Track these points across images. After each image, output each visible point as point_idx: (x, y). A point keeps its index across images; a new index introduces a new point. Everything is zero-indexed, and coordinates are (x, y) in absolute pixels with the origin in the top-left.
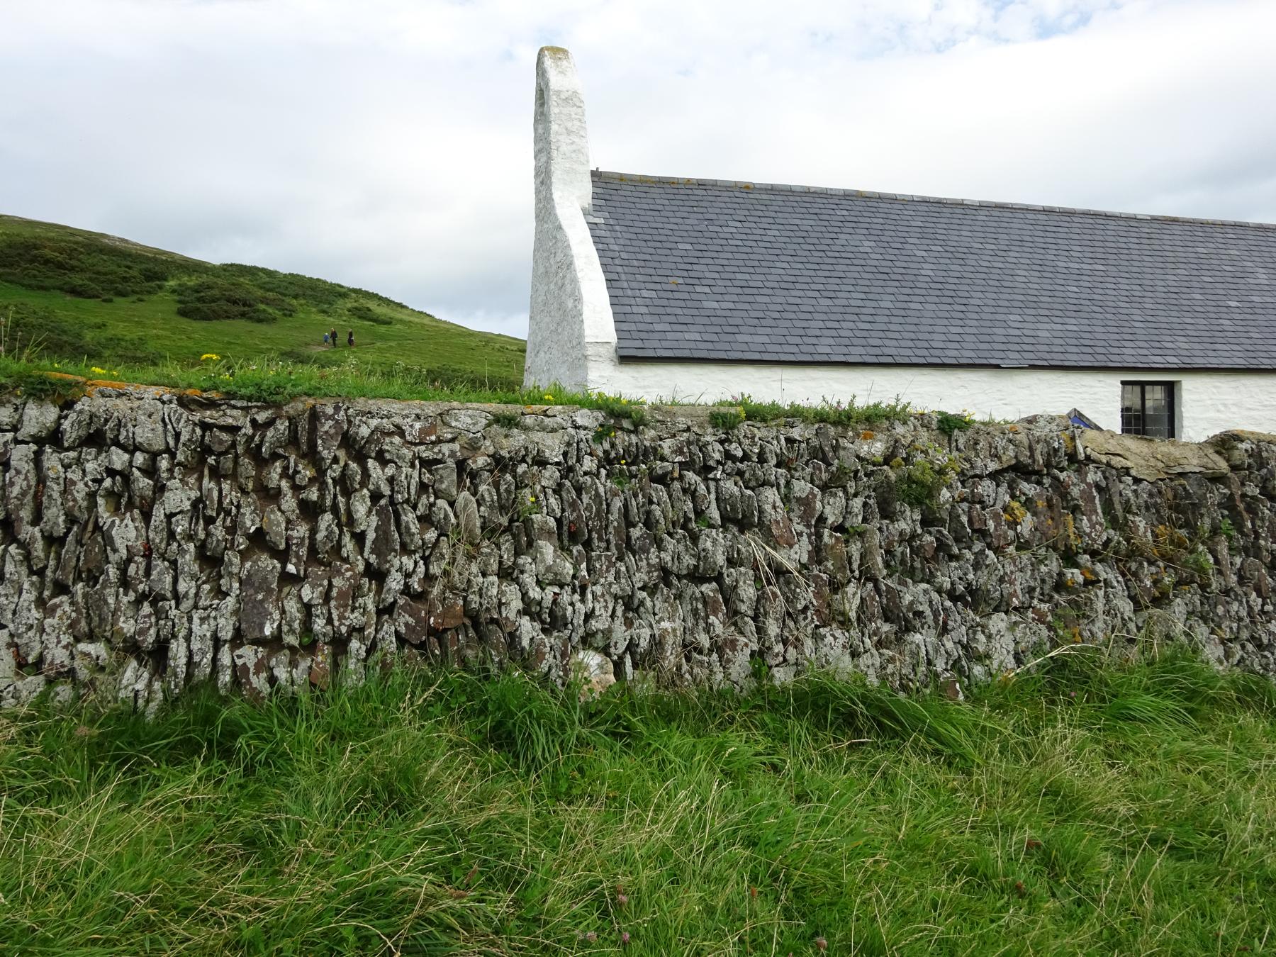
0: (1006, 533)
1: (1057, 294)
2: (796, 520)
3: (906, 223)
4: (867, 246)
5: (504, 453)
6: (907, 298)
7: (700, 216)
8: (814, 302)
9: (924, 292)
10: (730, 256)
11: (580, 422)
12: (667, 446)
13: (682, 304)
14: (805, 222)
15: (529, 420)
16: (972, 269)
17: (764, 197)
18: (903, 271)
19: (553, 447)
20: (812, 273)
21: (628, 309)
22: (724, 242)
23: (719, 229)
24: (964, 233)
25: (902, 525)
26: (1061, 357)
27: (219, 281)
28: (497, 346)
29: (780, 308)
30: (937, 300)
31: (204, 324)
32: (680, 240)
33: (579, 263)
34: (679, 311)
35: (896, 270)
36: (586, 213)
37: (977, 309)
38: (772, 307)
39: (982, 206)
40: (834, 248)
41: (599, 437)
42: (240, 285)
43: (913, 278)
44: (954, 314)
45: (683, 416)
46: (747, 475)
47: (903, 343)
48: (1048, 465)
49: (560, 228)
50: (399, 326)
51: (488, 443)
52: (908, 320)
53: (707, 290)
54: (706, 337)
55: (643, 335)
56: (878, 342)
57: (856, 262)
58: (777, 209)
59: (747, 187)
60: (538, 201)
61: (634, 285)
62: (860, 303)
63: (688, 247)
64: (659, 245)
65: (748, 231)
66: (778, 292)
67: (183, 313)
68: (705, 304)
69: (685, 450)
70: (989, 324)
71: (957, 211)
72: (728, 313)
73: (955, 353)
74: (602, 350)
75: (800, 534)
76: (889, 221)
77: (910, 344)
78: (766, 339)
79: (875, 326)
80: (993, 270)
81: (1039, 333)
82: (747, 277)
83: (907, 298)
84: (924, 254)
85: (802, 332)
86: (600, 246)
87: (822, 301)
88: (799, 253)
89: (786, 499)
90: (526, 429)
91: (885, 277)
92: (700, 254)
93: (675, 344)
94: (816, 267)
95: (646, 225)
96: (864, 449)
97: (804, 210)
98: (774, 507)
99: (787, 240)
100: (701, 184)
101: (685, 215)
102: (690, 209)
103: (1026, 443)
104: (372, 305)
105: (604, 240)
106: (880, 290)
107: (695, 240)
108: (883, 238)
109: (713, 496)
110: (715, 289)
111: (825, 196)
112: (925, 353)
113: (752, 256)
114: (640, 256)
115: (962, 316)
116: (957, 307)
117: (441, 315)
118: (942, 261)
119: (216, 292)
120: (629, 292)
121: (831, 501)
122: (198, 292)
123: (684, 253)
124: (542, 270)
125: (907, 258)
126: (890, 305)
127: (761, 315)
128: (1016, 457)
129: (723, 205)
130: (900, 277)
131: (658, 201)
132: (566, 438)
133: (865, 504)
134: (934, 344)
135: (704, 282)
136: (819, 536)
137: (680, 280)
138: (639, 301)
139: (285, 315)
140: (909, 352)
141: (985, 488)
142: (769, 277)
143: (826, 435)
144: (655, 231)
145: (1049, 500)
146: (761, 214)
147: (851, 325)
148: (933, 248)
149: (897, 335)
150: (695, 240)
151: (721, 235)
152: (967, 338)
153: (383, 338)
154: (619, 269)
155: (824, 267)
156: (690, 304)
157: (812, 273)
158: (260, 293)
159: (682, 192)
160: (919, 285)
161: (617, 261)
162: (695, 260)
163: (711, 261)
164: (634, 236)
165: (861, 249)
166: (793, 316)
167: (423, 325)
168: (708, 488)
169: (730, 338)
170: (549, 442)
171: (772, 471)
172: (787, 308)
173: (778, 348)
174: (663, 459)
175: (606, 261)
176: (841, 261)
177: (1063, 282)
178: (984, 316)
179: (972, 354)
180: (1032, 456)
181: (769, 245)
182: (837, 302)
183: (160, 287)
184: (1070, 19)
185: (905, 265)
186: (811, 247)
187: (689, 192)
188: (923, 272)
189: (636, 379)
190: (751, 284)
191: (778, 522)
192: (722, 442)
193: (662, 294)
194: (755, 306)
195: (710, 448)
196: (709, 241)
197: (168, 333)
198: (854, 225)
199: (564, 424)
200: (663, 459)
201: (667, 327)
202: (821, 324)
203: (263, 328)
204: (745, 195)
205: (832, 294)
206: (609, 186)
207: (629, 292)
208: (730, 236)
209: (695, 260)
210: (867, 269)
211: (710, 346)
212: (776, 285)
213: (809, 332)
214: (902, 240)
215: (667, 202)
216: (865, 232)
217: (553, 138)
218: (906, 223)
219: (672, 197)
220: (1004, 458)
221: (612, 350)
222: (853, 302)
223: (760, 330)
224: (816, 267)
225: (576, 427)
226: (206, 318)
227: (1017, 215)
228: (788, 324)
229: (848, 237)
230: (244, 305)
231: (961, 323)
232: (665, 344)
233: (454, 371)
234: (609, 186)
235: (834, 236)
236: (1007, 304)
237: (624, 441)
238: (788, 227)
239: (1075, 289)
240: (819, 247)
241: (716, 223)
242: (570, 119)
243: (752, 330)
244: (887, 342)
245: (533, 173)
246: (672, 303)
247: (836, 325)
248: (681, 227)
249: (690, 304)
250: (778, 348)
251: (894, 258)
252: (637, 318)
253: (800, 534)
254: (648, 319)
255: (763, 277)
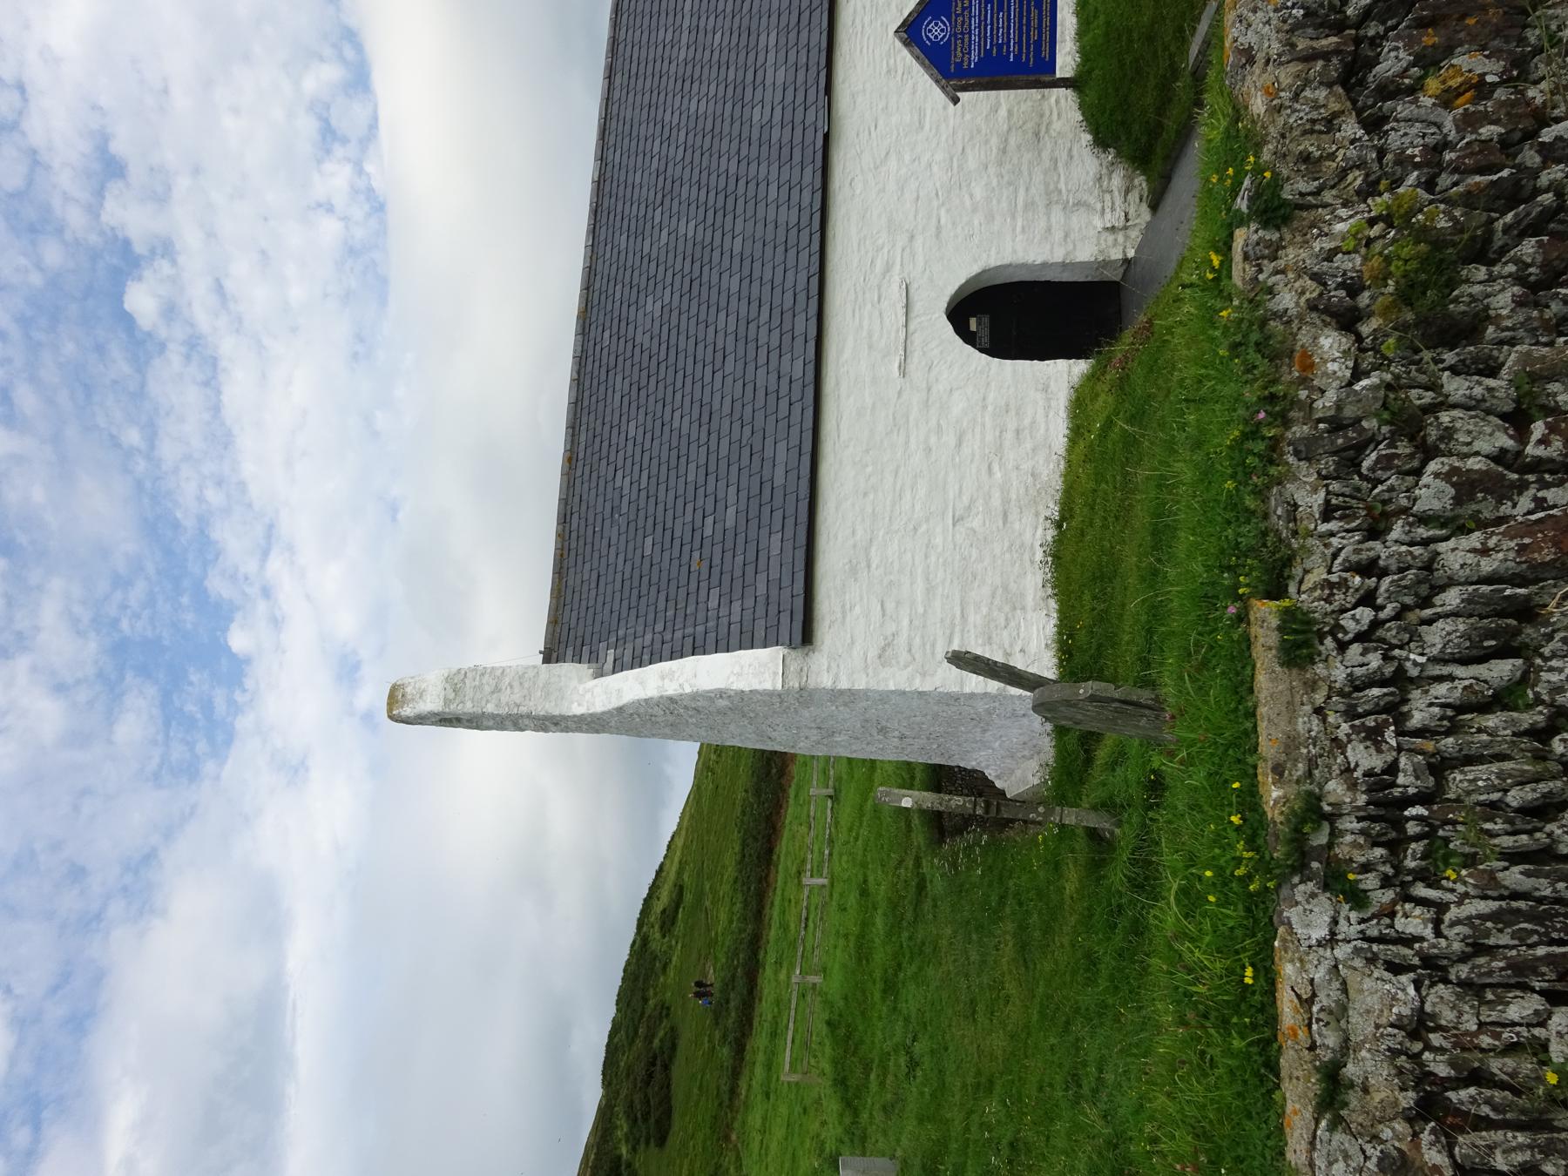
0: (1502, 104)
1: (724, 59)
2: (1506, 509)
3: (623, 254)
4: (652, 306)
5: (1408, 1099)
6: (727, 256)
7: (607, 523)
8: (729, 380)
9: (718, 234)
10: (662, 487)
11: (1320, 932)
12: (1364, 757)
13: (729, 555)
14: (618, 387)
15: (1331, 1039)
16: (688, 170)
17: (583, 438)
18: (688, 260)
19: (1381, 998)
20: (689, 381)
21: (735, 628)
22: (643, 494)
23: (625, 500)
24: (638, 181)
25: (1503, 301)
26: (814, 52)
27: (623, 1093)
28: (713, 757)
29: (737, 425)
30: (729, 218)
31: (676, 1116)
32: (639, 552)
33: (671, 689)
34: (739, 559)
35: (687, 269)
36: (600, 674)
37: (744, 163)
38: (735, 436)
39: (602, 158)
40: (655, 350)
41: (1358, 899)
42: (629, 1068)
43: (699, 248)
44: (751, 193)
45: (1292, 720)
46: (1408, 600)
47: (791, 262)
48: (1339, 27)
49: (620, 710)
50: (686, 877)
51: (1387, 1134)
52: (757, 255)
53: (709, 520)
54: (777, 526)
55: (773, 609)
56: (789, 295)
57: (674, 322)
58: (599, 422)
59: (570, 460)
60: (579, 730)
61: (701, 617)
62: (732, 319)
63: (649, 541)
64: (645, 580)
65: (629, 461)
66: (715, 426)
67: (662, 1140)
68: (730, 523)
69: (1370, 722)
70: (765, 148)
71: (607, 189)
72: (743, 494)
73: (807, 194)
74: (793, 667)
75: (1540, 504)
76: (620, 277)
77: (792, 253)
78: (782, 446)
79: (766, 297)
80: (690, 143)
81: (780, 82)
82: (692, 466)
83: (727, 256)
84: (665, 233)
85: (772, 398)
86: (646, 657)
87: (729, 368)
88: (660, 396)
89: (1457, 527)
90: (1346, 1047)
91: (696, 284)
92: (659, 528)
93: (787, 570)
94: (680, 374)
95: (618, 595)
96: (1339, 368)
97: (602, 388)
98: (1485, 551)
99: (642, 411)
100: (564, 518)
101: (605, 542)
102: (598, 535)
103: (1294, 68)
104: (658, 907)
105: (638, 652)
106: (714, 291)
107: (640, 532)
108: (643, 286)
109: (1459, 671)
110: (710, 508)
111: (582, 360)
112: (805, 234)
113: (664, 459)
114: (661, 605)
115: (752, 185)
116: (741, 190)
117: (670, 821)
118: (675, 210)
119: (637, 1098)
120: (711, 624)
121: (1463, 438)
122: (636, 1120)
123: (658, 548)
124: (667, 731)
125: (671, 255)
126: (736, 278)
127: (746, 452)
128: (1330, 85)
129: (593, 492)
130: (697, 265)
131: (586, 577)
132: (1358, 963)
133: (1454, 371)
134: (793, 220)
135: (698, 523)
136: (1538, 465)
137: (696, 555)
138: (724, 611)
139: (667, 1015)
140: (804, 255)
141: (1405, 138)
142: (694, 437)
143: (1311, 442)
144: (627, 583)
145: (1421, 24)
146: (605, 444)
147: (764, 331)
148: (657, 220)
149: (779, 271)
150: (640, 532)
151: (634, 497)
152: (785, 177)
153: (700, 896)
154: (679, 634)
155: (680, 365)
156: (729, 544)
157: (689, 381)
158: (639, 1043)
159: (573, 545)
160: (708, 240)
161: (668, 637)
162: (668, 533)
163: (670, 513)
164: (633, 612)
165: (657, 314)
166: (748, 409)
167: (685, 846)
168: (1440, 679)
169: (779, 494)
170: (1373, 1001)
171: (1393, 546)
172: (737, 415)
173: (795, 431)
174: (1392, 769)
175: (666, 652)
176: (673, 341)
177: (707, 52)
178: (754, 154)
179: (808, 171)
180: (1326, 56)
181: (649, 435)
182: (730, 348)
183: (629, 1165)
184: (349, 53)
185: (679, 258)
186: (653, 380)
187: (574, 535)
188: (690, 234)
189: (832, 622)
190: (702, 461)
191: (1522, 549)
192: (1342, 647)
193: (715, 580)
194: (734, 457)
195: (1359, 671)
196: (642, 513)
197: (686, 1162)
198: (623, 324)
199: (1327, 964)
200: (1392, 769)
201: (762, 577)
202: (762, 372)
203: (682, 1044)
204: (580, 463)
205: (719, 355)
206: (564, 638)
207: (711, 624)
208: (635, 485)
209: (668, 533)
210: (684, 307)
211: (790, 522)
212: (705, 428)
213: (772, 388)
214: (646, 260)
215: (587, 566)
216: (633, 308)
217: (503, 711)
218: (623, 254)
219: (580, 558)
220: (1335, 106)
221: (794, 654)
222: (731, 328)
223: (769, 453)
224: (680, 374)
225: (1332, 940)
226: (668, 1113)
227: (615, 112)
228: (760, 415)
229: (640, 330)
230: (654, 1064)
231: (763, 186)
232: (786, 582)
233: (744, 813)
234: (564, 638)
235: (638, 350)
236: (737, 125)
237: (1355, 845)
238: (625, 410)
239: (718, 35)
240: (653, 370)
241: (616, 503)
242: (480, 688)
243: (768, 465)
244: (789, 283)
245: (541, 734)
246: (727, 567)
247: (763, 352)
248: (622, 548)
249: (729, 544)
250: (795, 431)
251: (670, 273)
252: (748, 615)
253: (1540, 504)
254: (749, 603)
255: (694, 447)
